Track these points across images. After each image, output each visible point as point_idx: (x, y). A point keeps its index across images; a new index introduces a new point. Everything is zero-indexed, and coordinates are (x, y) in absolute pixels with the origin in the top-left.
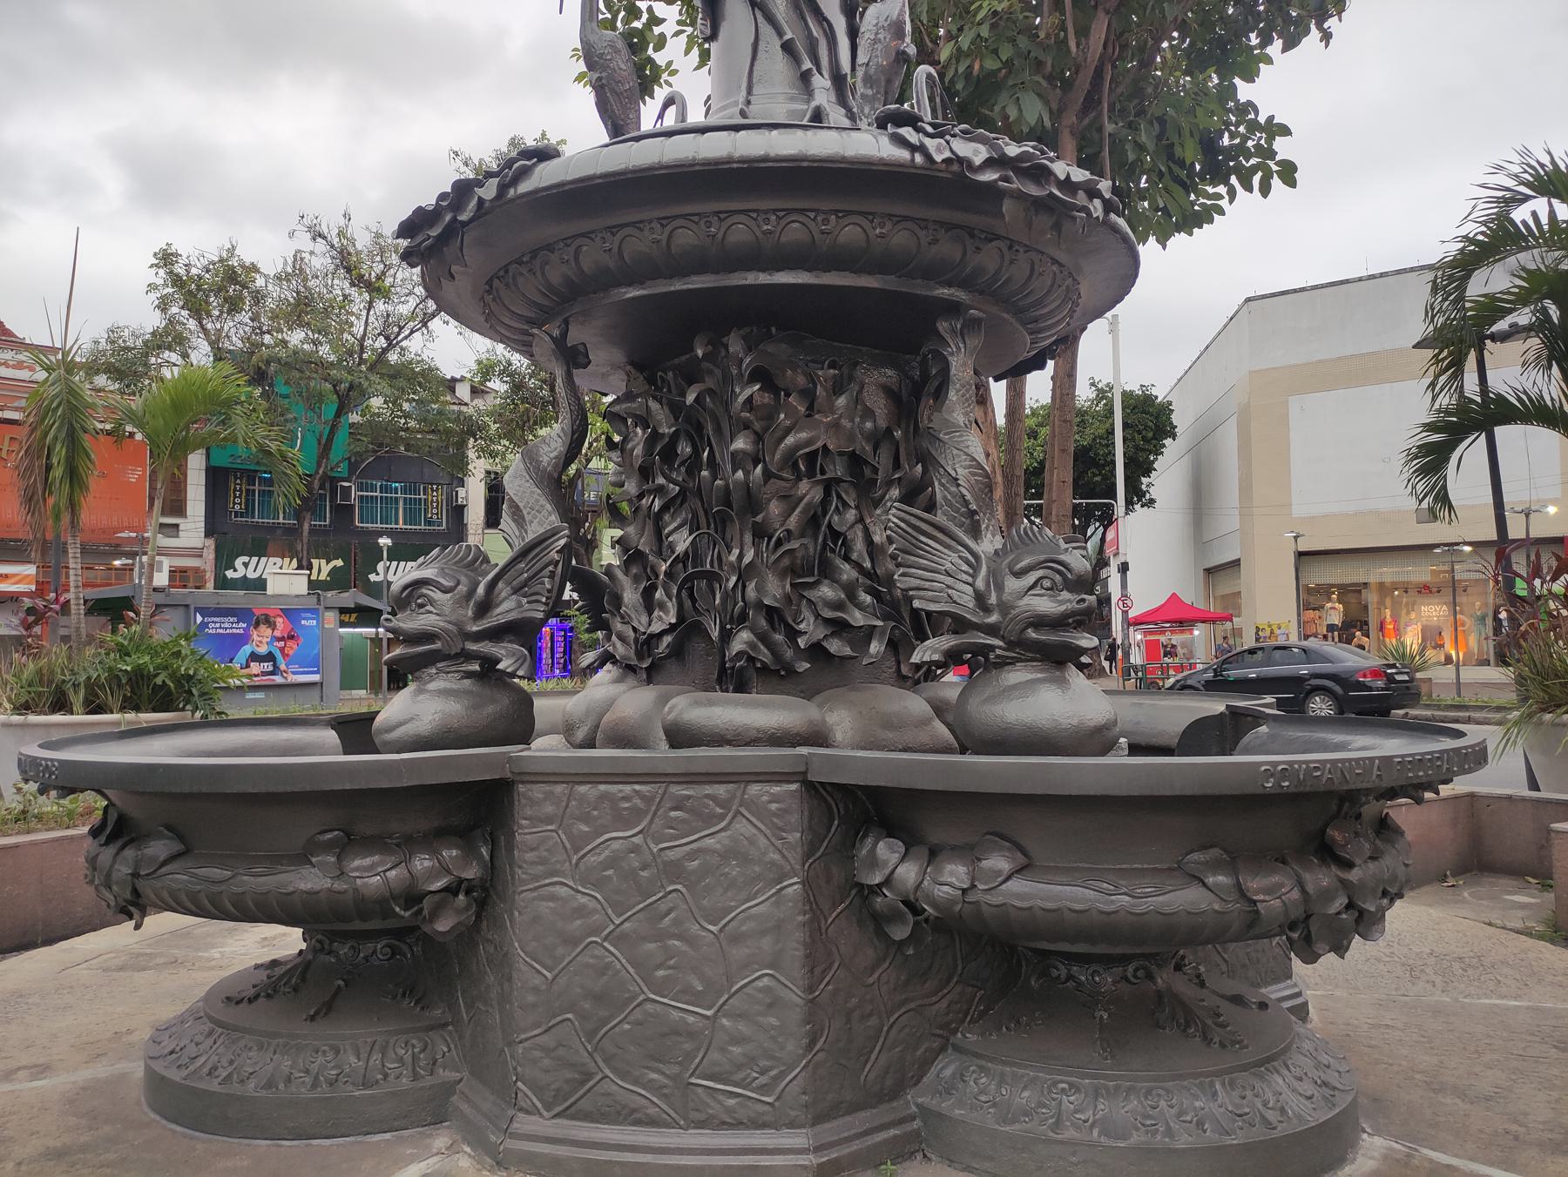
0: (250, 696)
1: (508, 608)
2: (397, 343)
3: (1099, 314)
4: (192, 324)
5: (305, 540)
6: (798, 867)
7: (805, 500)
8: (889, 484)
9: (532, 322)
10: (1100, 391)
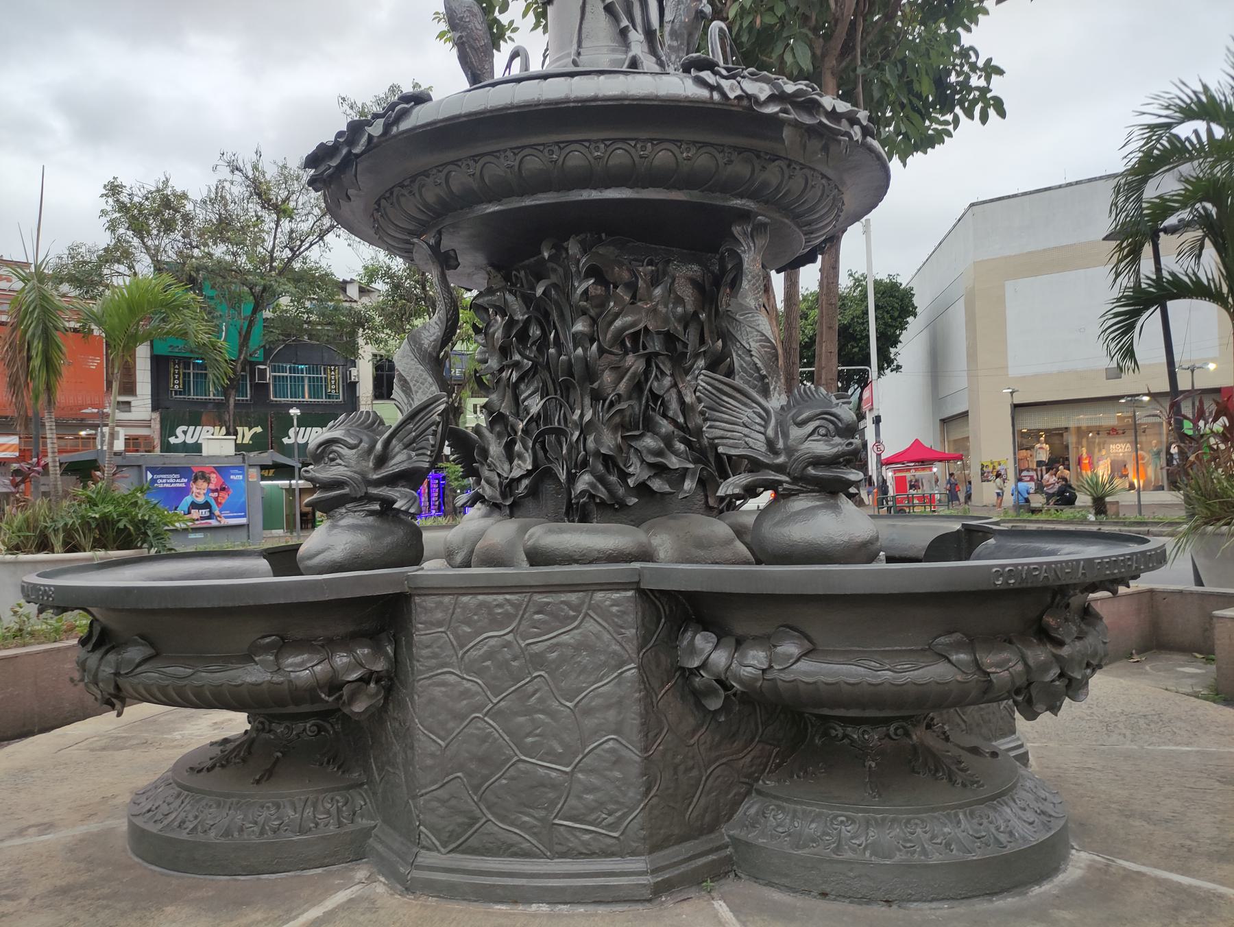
0: (192, 536)
1: (400, 460)
2: (300, 254)
3: (857, 218)
4: (136, 242)
5: (232, 413)
6: (634, 656)
7: (631, 371)
8: (697, 356)
9: (412, 233)
10: (856, 280)
